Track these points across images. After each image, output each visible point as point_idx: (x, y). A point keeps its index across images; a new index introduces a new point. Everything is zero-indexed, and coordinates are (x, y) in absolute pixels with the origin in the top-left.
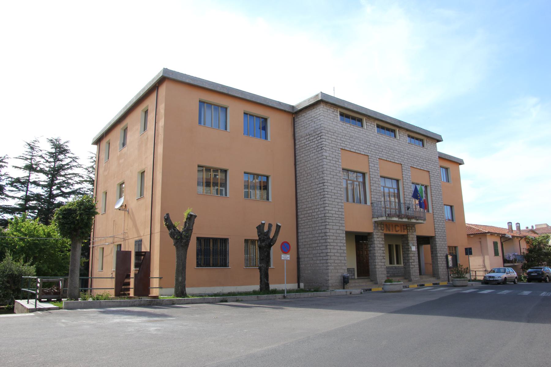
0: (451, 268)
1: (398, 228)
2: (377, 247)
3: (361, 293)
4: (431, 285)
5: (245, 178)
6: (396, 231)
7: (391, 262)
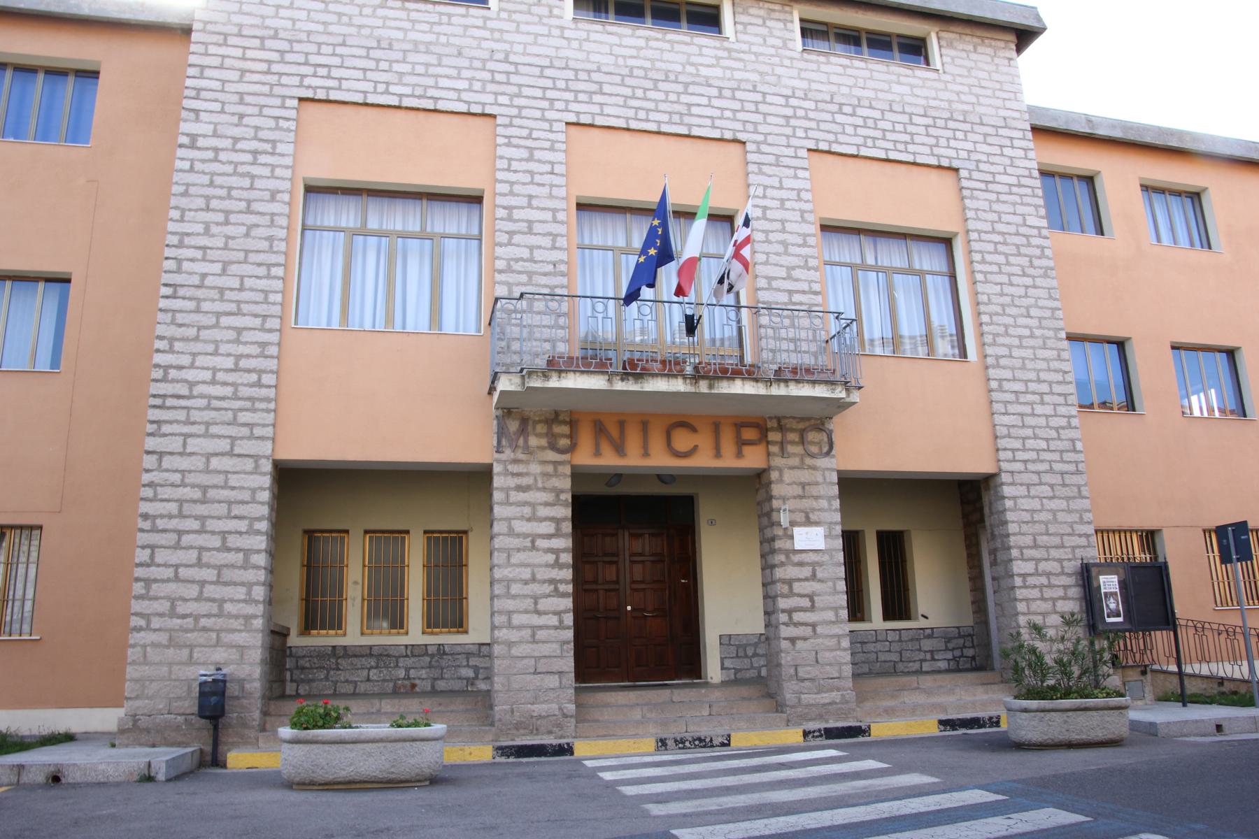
0: (1117, 631)
1: (682, 440)
2: (511, 533)
3: (148, 778)
4: (932, 729)
5: (1068, 360)
6: (678, 455)
7: (857, 609)
